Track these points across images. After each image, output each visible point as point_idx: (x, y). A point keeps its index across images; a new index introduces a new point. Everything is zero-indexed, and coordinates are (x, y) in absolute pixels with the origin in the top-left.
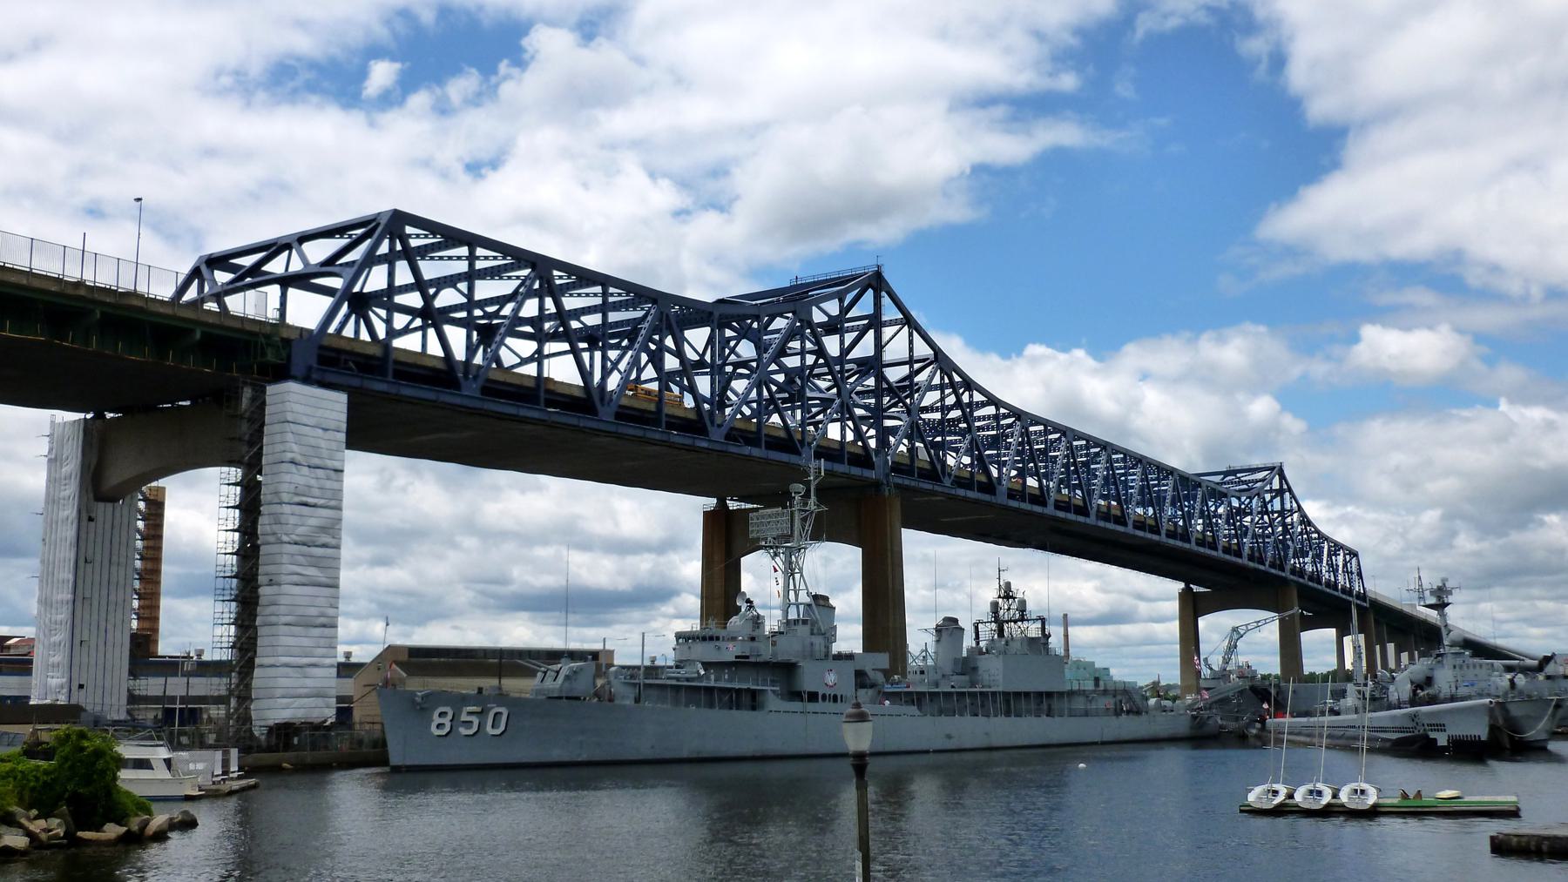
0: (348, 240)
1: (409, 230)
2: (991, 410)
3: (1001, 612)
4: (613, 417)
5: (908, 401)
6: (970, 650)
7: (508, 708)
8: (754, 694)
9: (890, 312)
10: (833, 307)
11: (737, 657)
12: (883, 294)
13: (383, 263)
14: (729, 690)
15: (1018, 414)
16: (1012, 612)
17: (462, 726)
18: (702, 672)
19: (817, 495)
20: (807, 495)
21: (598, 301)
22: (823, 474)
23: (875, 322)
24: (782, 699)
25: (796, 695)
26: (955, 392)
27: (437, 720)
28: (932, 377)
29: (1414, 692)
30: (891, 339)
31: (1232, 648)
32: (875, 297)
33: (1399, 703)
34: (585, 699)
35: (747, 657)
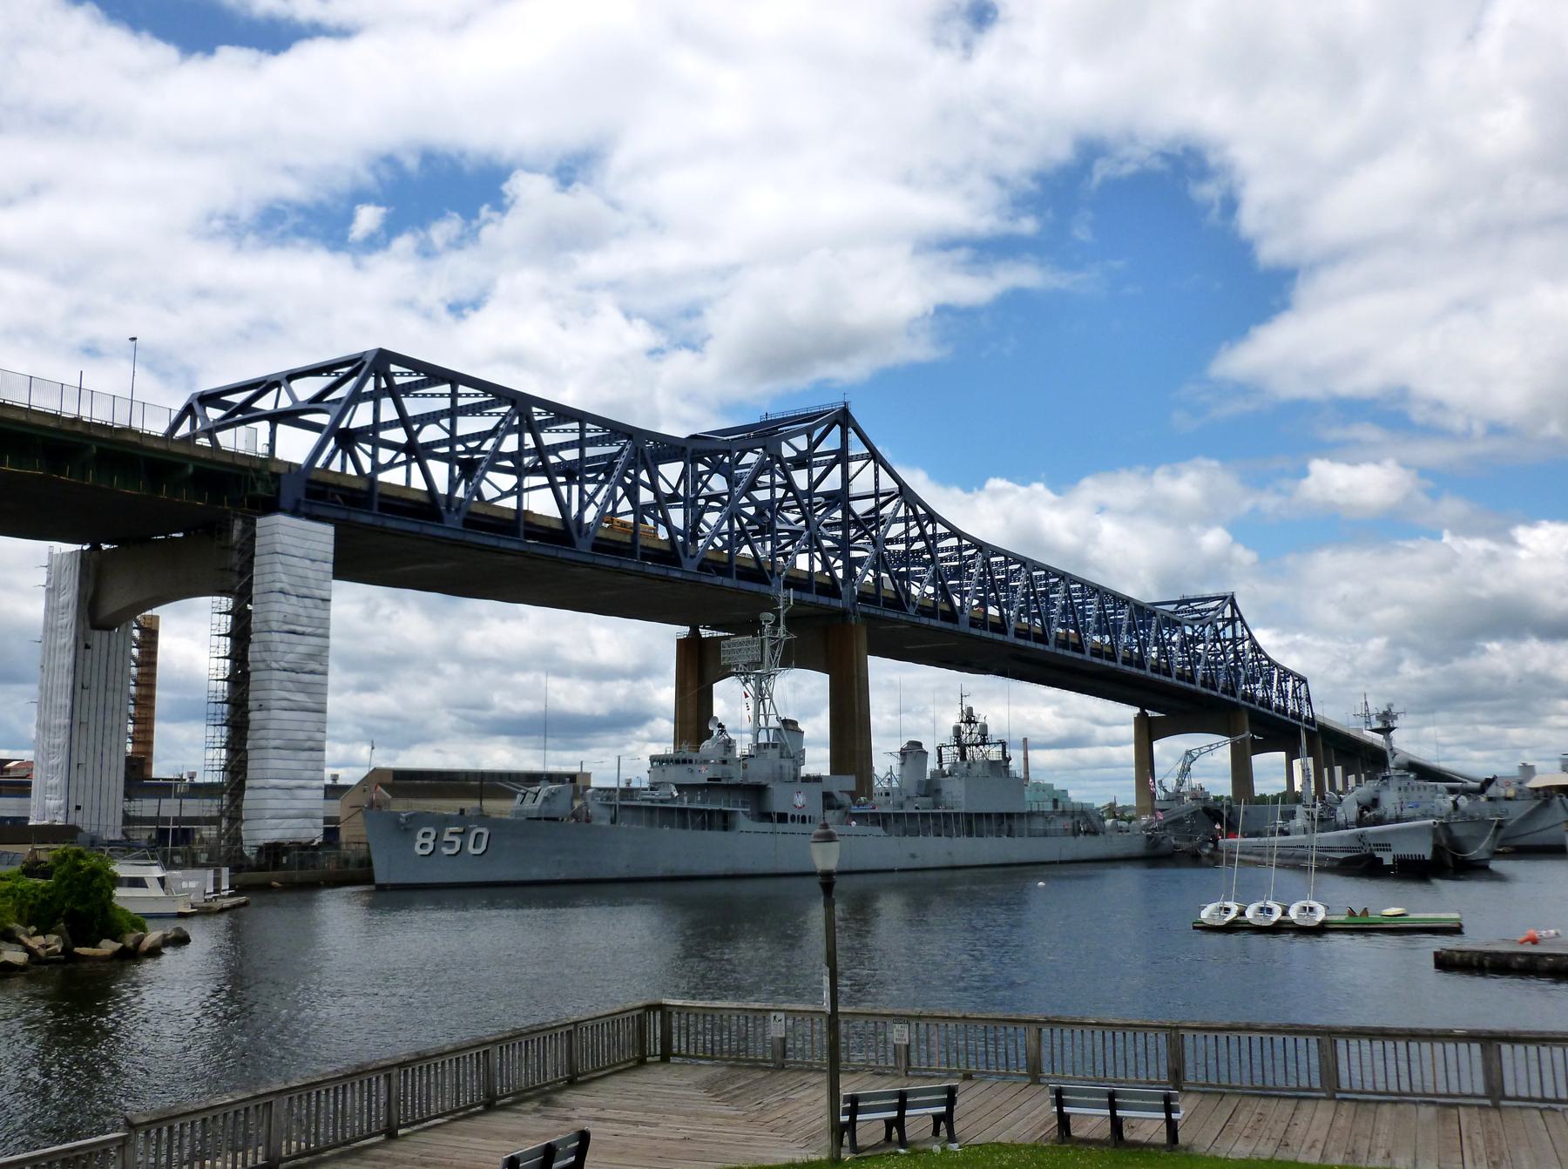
0: (335, 378)
1: (394, 368)
3: (964, 736)
5: (874, 533)
6: (934, 773)
9: (857, 447)
10: (801, 443)
11: (709, 780)
12: (850, 430)
14: (701, 811)
15: (979, 546)
18: (676, 794)
19: (786, 623)
20: (776, 624)
21: (576, 436)
23: (842, 457)
24: (753, 820)
25: (765, 816)
26: (919, 524)
27: (420, 840)
28: (896, 510)
29: (1361, 813)
30: (857, 473)
31: (1185, 771)
35: (719, 780)
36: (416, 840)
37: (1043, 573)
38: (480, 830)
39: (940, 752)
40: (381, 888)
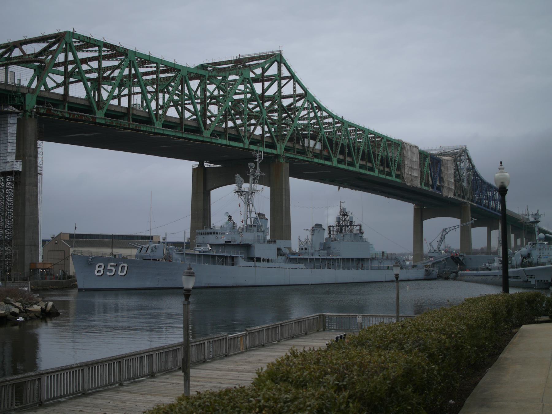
0: (48, 44)
2: (330, 120)
3: (341, 222)
4: (161, 126)
5: (293, 116)
6: (326, 239)
7: (104, 264)
8: (233, 258)
10: (258, 71)
11: (225, 242)
12: (282, 65)
13: (63, 53)
14: (222, 256)
16: (346, 222)
17: (108, 272)
18: (210, 249)
19: (260, 168)
20: (256, 168)
22: (263, 158)
24: (245, 261)
25: (251, 259)
26: (314, 111)
27: (97, 269)
28: (303, 105)
29: (523, 261)
31: (443, 238)
32: (278, 66)
33: (516, 265)
34: (159, 260)
35: (230, 242)
36: (96, 269)
37: (373, 136)
38: (124, 265)
39: (329, 229)
40: (80, 290)
